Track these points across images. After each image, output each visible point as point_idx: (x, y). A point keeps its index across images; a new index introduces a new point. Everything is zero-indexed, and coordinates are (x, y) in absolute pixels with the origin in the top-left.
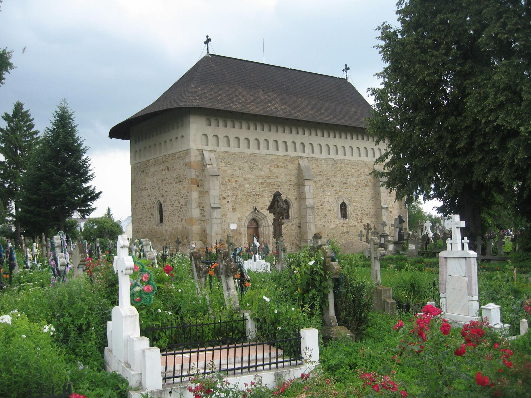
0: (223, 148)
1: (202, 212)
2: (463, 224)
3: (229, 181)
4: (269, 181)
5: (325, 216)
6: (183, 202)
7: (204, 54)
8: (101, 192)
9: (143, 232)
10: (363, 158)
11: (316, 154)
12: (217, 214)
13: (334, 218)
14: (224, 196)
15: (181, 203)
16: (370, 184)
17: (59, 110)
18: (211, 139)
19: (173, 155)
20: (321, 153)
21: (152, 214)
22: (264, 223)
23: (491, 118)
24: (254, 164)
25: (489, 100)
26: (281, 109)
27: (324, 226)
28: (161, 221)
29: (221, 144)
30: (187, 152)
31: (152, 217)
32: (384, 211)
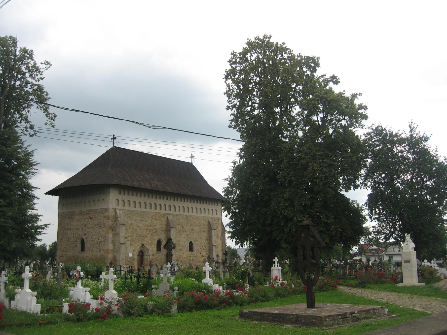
0: (127, 208)
2: (278, 260)
4: (151, 228)
5: (181, 250)
6: (101, 239)
9: (67, 256)
11: (177, 212)
12: (123, 247)
15: (100, 240)
16: (206, 230)
18: (121, 203)
19: (96, 210)
20: (180, 211)
21: (76, 246)
23: (283, 212)
25: (282, 204)
28: (83, 249)
30: (107, 210)
31: (75, 248)
32: (214, 248)
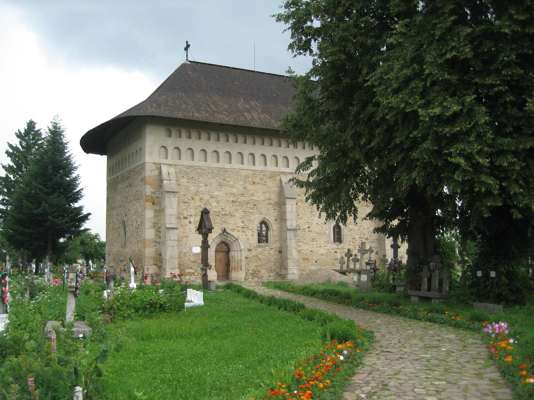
1: (158, 233)
3: (193, 198)
4: (241, 199)
5: (313, 240)
7: (184, 61)
8: (89, 214)
10: (282, 168)
13: (325, 242)
14: (186, 216)
17: (51, 127)
22: (235, 247)
24: (224, 180)
26: (259, 118)
27: (312, 251)
29: (233, 160)
